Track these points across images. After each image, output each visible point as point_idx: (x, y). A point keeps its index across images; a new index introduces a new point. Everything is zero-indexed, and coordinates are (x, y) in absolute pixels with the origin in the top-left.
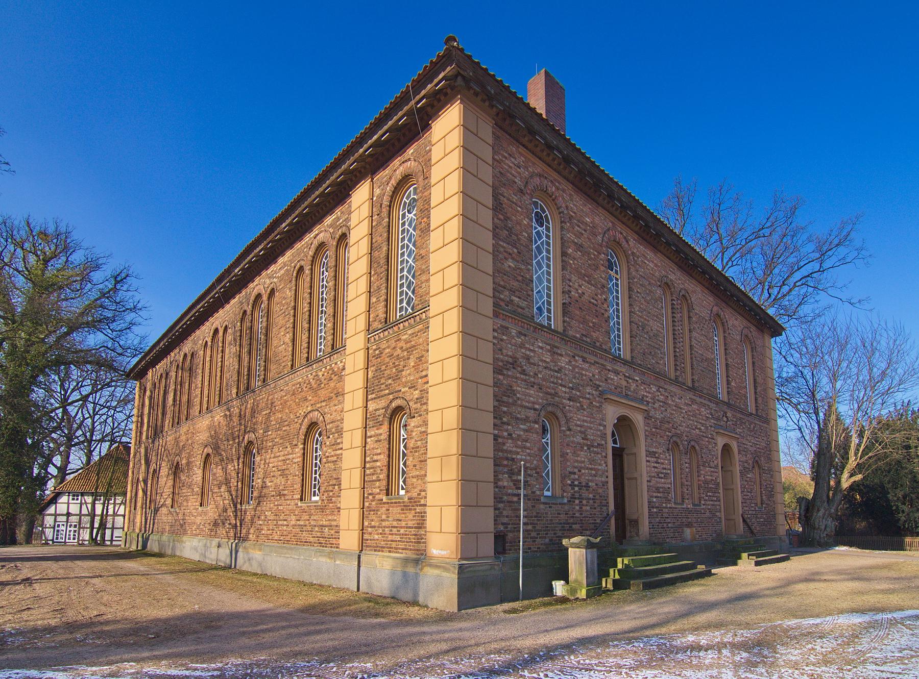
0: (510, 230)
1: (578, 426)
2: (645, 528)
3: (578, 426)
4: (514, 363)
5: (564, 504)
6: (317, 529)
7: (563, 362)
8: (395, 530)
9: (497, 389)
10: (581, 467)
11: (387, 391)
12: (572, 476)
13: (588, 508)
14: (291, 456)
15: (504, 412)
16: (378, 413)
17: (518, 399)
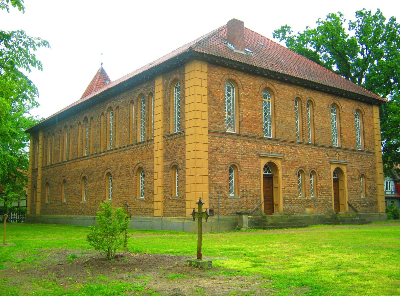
0: (215, 100)
1: (246, 169)
2: (281, 207)
3: (246, 169)
4: (217, 149)
5: (239, 199)
6: (143, 209)
7: (239, 145)
8: (175, 209)
9: (210, 160)
10: (247, 185)
11: (171, 159)
12: (243, 188)
13: (250, 200)
14: (130, 181)
15: (213, 167)
16: (167, 167)
17: (219, 162)
